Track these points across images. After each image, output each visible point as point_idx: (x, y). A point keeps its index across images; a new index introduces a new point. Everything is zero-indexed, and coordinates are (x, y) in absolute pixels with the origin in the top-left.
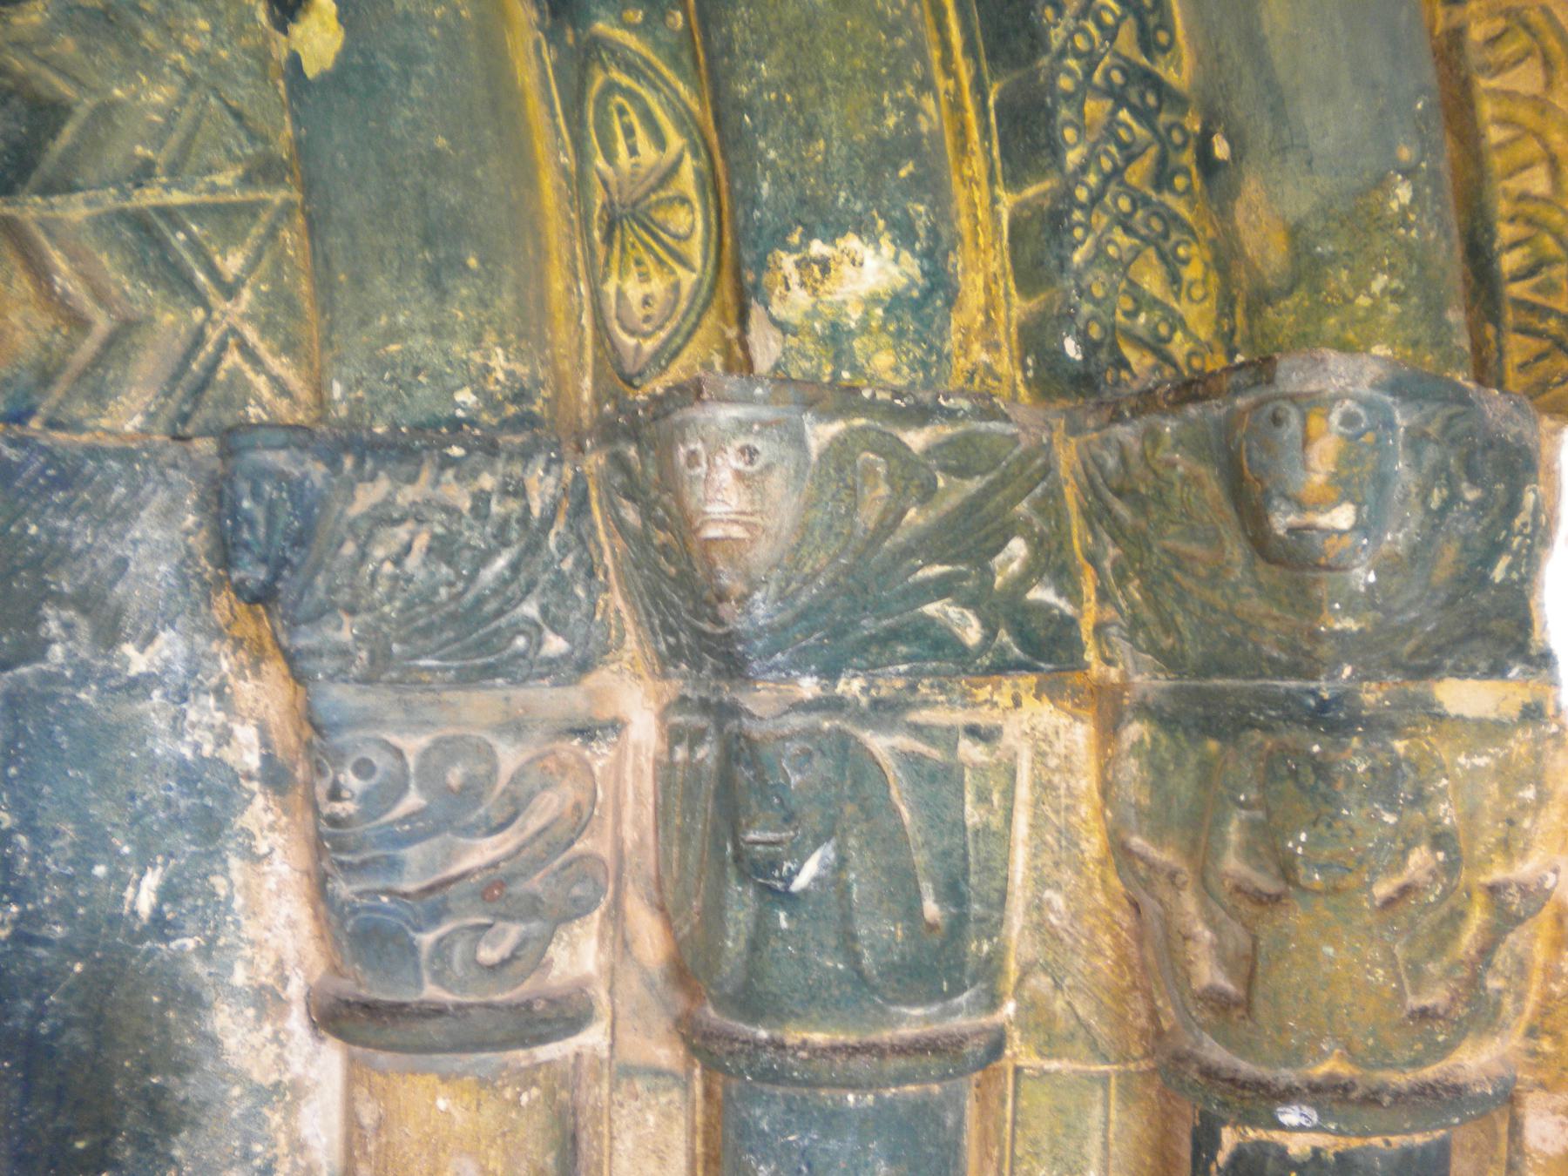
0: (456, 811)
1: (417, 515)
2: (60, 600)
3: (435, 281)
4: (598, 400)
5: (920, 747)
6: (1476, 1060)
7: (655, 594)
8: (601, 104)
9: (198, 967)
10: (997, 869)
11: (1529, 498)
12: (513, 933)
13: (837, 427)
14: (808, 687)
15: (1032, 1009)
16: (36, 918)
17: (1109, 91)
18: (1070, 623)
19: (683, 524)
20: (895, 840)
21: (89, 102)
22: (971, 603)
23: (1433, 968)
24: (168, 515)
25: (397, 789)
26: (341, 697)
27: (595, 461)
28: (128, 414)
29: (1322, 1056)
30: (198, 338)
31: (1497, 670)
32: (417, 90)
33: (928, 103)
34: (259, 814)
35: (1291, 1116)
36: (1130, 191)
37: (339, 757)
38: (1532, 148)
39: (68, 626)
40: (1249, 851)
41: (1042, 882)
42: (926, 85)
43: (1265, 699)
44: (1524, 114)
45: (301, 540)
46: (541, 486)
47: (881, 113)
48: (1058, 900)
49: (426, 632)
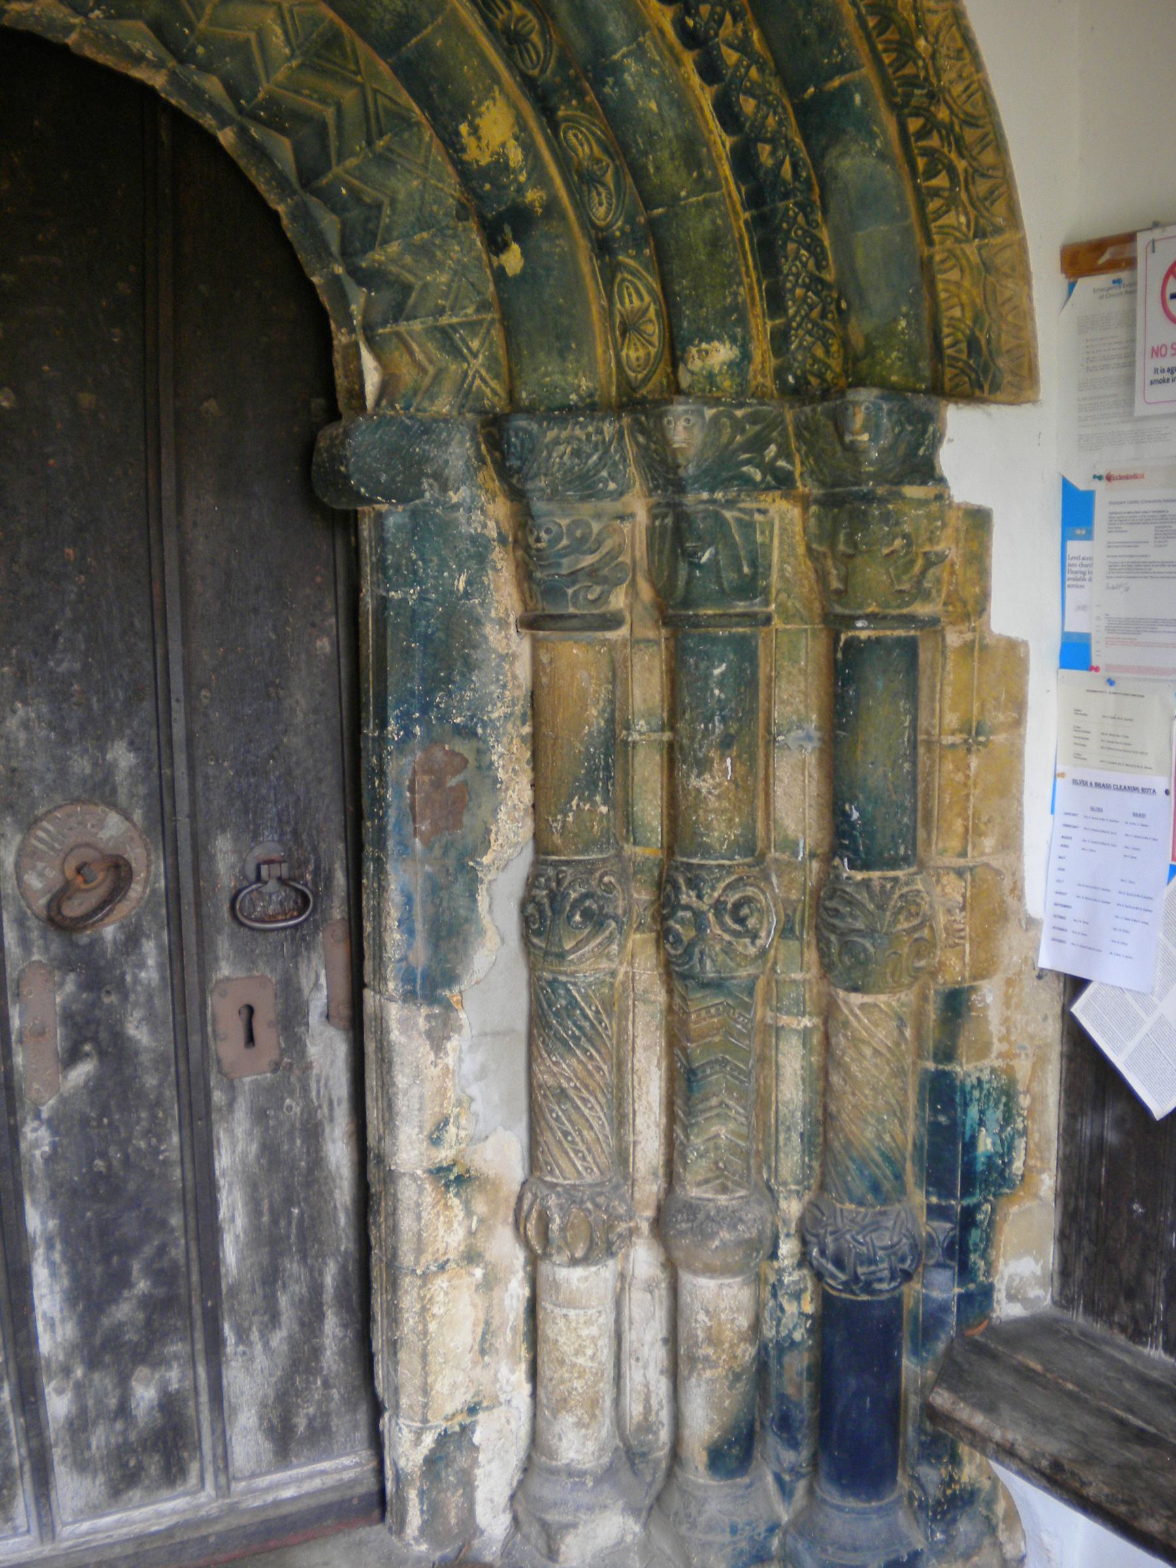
0: (580, 545)
1: (568, 442)
2: (428, 476)
3: (563, 359)
4: (619, 394)
5: (741, 515)
6: (922, 609)
7: (650, 467)
8: (620, 285)
9: (479, 610)
10: (768, 556)
11: (931, 429)
12: (598, 590)
13: (714, 411)
14: (705, 495)
15: (779, 606)
16: (426, 591)
17: (804, 286)
19: (665, 442)
20: (734, 545)
21: (420, 283)
22: (758, 466)
23: (905, 578)
24: (461, 443)
25: (559, 538)
27: (626, 420)
28: (443, 405)
29: (869, 605)
30: (466, 374)
31: (924, 483)
32: (552, 282)
33: (741, 290)
34: (498, 554)
35: (859, 624)
36: (811, 321)
38: (956, 300)
39: (431, 485)
40: (846, 543)
41: (782, 561)
42: (740, 283)
43: (850, 493)
44: (952, 288)
47: (725, 298)
48: (789, 569)
49: (570, 482)
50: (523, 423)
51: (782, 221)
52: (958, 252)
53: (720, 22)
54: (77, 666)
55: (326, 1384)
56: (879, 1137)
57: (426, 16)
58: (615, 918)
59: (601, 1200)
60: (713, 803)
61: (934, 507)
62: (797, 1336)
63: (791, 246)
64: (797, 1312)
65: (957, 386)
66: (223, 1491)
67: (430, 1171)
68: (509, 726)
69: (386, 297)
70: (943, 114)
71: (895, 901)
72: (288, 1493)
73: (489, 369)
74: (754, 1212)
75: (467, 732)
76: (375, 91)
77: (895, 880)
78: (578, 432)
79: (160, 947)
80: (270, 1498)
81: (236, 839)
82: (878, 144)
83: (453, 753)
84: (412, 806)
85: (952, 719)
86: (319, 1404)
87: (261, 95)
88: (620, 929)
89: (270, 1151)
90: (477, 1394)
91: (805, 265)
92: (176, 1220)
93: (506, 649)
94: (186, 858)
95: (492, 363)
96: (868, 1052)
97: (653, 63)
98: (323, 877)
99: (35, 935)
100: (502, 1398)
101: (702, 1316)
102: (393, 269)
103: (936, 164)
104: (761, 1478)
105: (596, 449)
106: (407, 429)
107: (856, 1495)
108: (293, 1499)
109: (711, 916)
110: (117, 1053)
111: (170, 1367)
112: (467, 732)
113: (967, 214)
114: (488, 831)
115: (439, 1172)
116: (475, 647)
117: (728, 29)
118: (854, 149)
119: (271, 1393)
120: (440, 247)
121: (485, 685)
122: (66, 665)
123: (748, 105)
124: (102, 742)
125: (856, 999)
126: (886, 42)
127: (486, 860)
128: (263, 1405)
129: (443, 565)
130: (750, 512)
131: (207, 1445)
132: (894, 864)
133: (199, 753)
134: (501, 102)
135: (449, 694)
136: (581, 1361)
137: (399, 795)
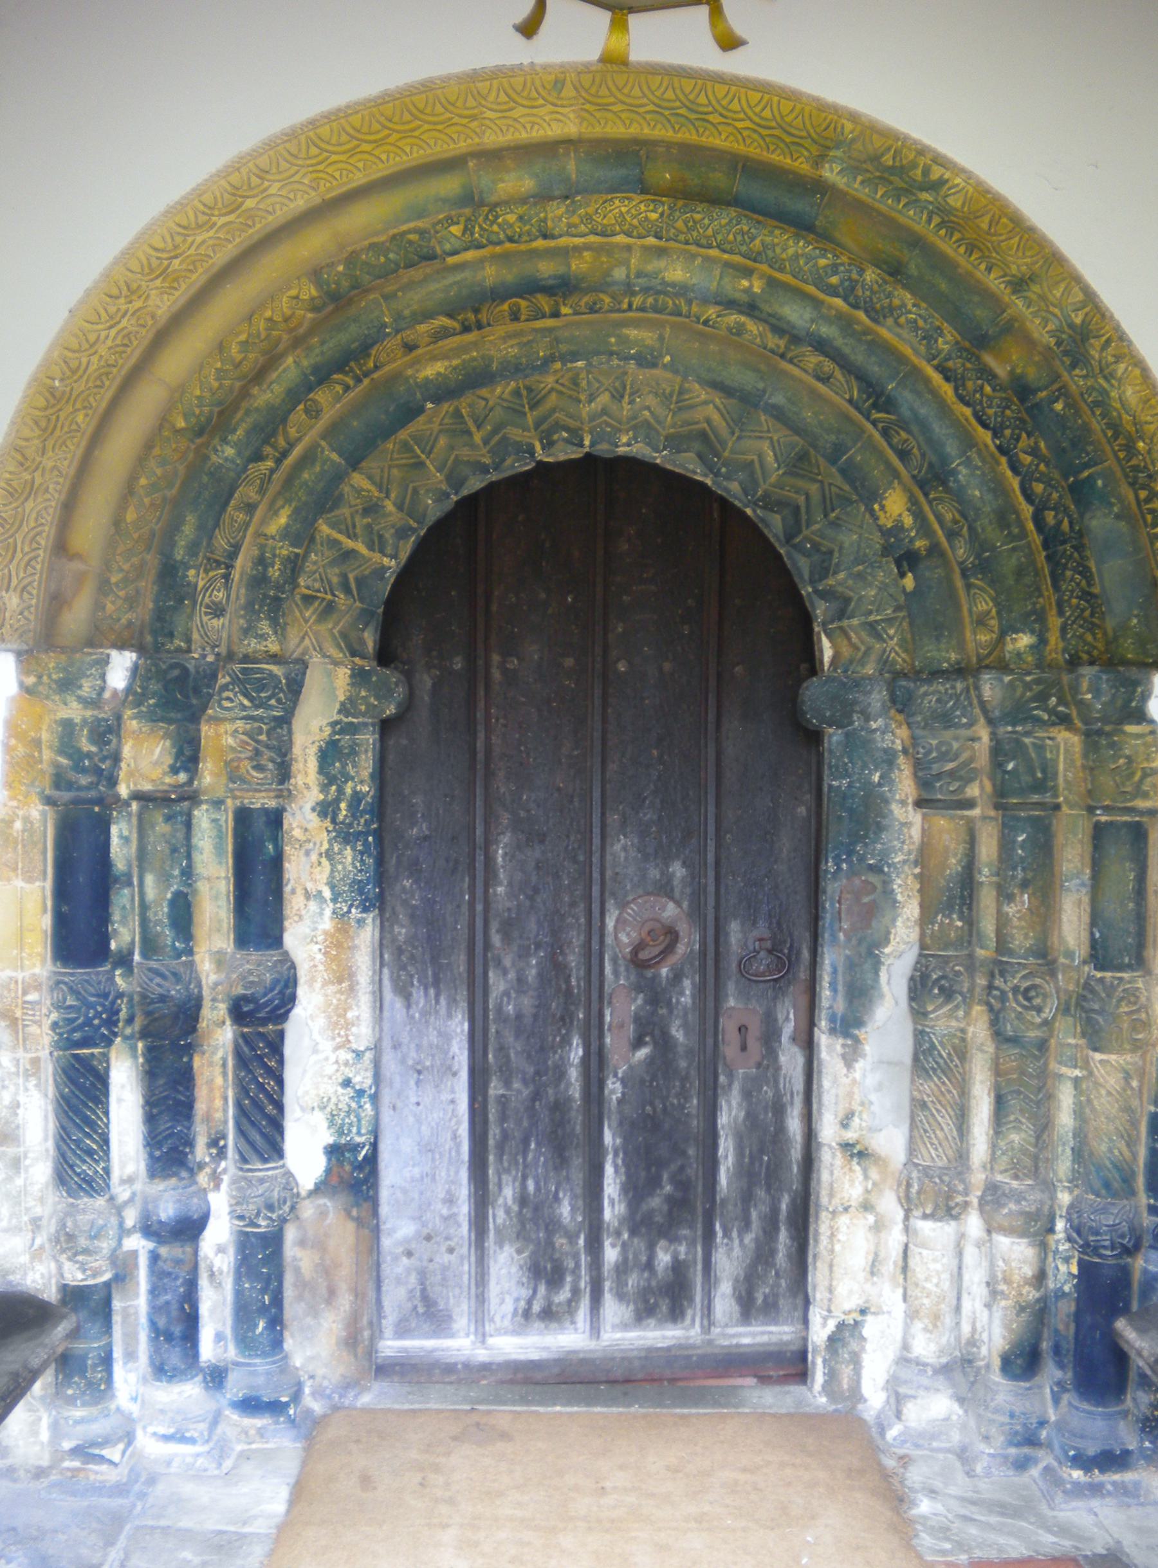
0: (944, 757)
1: (933, 693)
6: (1141, 804)
14: (1010, 728)
24: (880, 692)
25: (929, 752)
26: (919, 732)
28: (869, 670)
30: (884, 651)
31: (1139, 723)
34: (901, 760)
41: (1066, 770)
50: (904, 683)
53: (1018, 439)
54: (655, 817)
55: (777, 1274)
56: (1110, 1150)
58: (961, 994)
59: (946, 1178)
60: (1015, 922)
61: (1149, 739)
62: (1067, 1288)
63: (1069, 573)
64: (1065, 1272)
66: (706, 1329)
67: (840, 1145)
71: (1119, 993)
72: (746, 1341)
73: (901, 647)
74: (1036, 1196)
75: (876, 869)
77: (1121, 979)
78: (941, 688)
79: (693, 984)
80: (734, 1341)
81: (743, 924)
83: (866, 882)
84: (839, 913)
86: (772, 1287)
88: (964, 1001)
89: (751, 1117)
90: (867, 1301)
91: (1078, 584)
92: (691, 1152)
93: (907, 822)
94: (711, 932)
95: (903, 643)
96: (1103, 1092)
97: (977, 468)
98: (794, 952)
99: (622, 969)
100: (885, 1309)
101: (1001, 1263)
102: (840, 589)
104: (1040, 1387)
105: (951, 698)
106: (844, 684)
107: (1088, 1401)
108: (748, 1345)
109: (1010, 995)
110: (664, 1044)
111: (680, 1244)
112: (876, 869)
114: (889, 933)
115: (846, 1146)
117: (1024, 442)
119: (742, 1274)
122: (649, 815)
123: (1039, 488)
124: (667, 860)
125: (1098, 1056)
127: (887, 950)
128: (736, 1280)
129: (865, 766)
131: (698, 1298)
132: (1121, 968)
135: (866, 845)
136: (928, 1285)
137: (832, 905)
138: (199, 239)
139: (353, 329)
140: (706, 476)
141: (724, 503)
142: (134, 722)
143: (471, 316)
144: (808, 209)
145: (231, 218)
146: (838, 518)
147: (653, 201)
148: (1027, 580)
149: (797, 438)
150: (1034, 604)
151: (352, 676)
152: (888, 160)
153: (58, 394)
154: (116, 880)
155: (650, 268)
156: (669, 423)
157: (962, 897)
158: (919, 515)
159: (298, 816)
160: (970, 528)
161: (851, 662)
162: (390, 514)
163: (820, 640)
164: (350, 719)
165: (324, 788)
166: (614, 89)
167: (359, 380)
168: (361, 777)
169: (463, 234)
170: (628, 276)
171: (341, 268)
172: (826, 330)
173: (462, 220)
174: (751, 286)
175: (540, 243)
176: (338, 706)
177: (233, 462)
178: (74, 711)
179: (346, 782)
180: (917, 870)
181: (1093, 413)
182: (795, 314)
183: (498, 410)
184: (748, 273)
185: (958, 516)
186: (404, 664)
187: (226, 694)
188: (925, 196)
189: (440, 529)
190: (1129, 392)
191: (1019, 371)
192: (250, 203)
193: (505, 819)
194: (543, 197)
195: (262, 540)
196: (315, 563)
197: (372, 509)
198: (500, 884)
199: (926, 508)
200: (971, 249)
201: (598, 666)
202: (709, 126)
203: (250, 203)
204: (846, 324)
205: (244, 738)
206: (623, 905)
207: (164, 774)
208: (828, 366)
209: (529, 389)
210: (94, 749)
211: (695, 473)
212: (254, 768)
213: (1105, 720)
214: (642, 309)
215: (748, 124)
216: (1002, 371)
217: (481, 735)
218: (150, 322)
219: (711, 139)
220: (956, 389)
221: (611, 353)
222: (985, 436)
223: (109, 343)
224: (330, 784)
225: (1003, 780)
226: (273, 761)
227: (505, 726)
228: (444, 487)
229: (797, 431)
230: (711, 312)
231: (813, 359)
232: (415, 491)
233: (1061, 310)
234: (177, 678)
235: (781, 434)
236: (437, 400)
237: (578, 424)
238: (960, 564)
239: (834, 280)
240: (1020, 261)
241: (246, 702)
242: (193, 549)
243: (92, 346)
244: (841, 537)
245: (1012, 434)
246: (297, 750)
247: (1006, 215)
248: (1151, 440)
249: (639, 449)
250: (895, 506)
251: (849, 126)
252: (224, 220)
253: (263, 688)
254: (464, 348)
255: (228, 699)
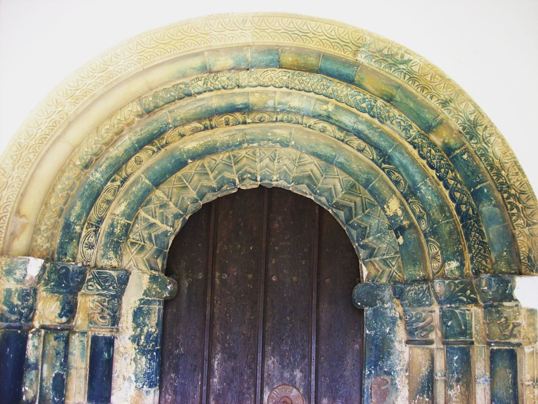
0: (418, 320)
2: (378, 300)
3: (414, 266)
6: (513, 341)
9: (393, 338)
11: (509, 285)
12: (425, 333)
14: (449, 306)
15: (476, 338)
17: (477, 244)
18: (476, 299)
22: (464, 297)
26: (406, 308)
28: (384, 280)
29: (495, 339)
30: (391, 272)
31: (510, 301)
34: (399, 322)
35: (492, 344)
37: (406, 314)
41: (475, 325)
44: (522, 242)
45: (402, 293)
46: (425, 287)
51: (469, 226)
52: (522, 231)
53: (448, 173)
57: (373, 179)
60: (454, 399)
61: (515, 309)
63: (473, 233)
65: (526, 271)
68: (402, 372)
69: (367, 252)
70: (513, 192)
73: (398, 270)
76: (365, 198)
82: (493, 202)
84: (371, 394)
85: (528, 376)
87: (334, 202)
91: (478, 238)
93: (402, 352)
95: (399, 268)
97: (430, 186)
102: (370, 244)
103: (513, 206)
106: (373, 287)
112: (388, 373)
113: (523, 220)
116: (391, 349)
117: (450, 175)
118: (486, 204)
120: (384, 237)
121: (394, 360)
123: (458, 195)
126: (494, 173)
129: (382, 324)
130: (464, 310)
133: (320, 375)
134: (395, 198)
135: (383, 362)
137: (368, 390)
138: (88, 82)
139: (155, 125)
140: (311, 195)
141: (321, 208)
142: (44, 293)
143: (208, 122)
144: (351, 73)
145: (103, 74)
146: (369, 213)
147: (285, 71)
148: (455, 237)
149: (351, 178)
150: (458, 248)
151: (150, 279)
152: (385, 52)
153: (22, 146)
154: (29, 366)
155: (284, 101)
156: (295, 173)
157: (428, 387)
158: (404, 210)
159: (123, 342)
160: (428, 215)
161: (376, 277)
162: (172, 208)
163: (362, 267)
164: (148, 298)
165: (135, 329)
166: (267, 23)
167: (159, 149)
168: (152, 325)
169: (203, 85)
170: (274, 104)
171: (151, 99)
172: (361, 127)
173: (203, 79)
174: (328, 108)
175: (237, 90)
176: (143, 292)
177: (99, 180)
178: (12, 285)
179: (145, 326)
180: (407, 374)
181: (481, 159)
182: (348, 120)
183: (221, 165)
184: (327, 103)
185: (422, 210)
186: (177, 275)
187: (90, 283)
188: (401, 66)
189: (195, 216)
190: (497, 149)
191: (446, 141)
192: (111, 68)
193: (219, 347)
194: (237, 69)
195: (113, 216)
196: (137, 228)
197: (163, 206)
198: (216, 377)
199: (408, 207)
200: (423, 88)
201: (263, 278)
202: (308, 38)
203: (111, 68)
204: (370, 125)
205: (98, 304)
206: (272, 390)
207: (56, 317)
208: (363, 144)
209: (234, 156)
210: (20, 303)
211: (306, 194)
212: (100, 317)
213: (494, 300)
214: (281, 121)
215: (325, 37)
216: (439, 142)
217: (208, 309)
218: (66, 117)
219: (309, 45)
220: (419, 151)
221: (269, 140)
222: (433, 173)
223: (47, 125)
224: (138, 327)
225: (446, 330)
226: (109, 314)
227: (220, 304)
228: (196, 196)
229: (350, 174)
230: (312, 121)
231: (357, 142)
232: (183, 198)
233: (464, 114)
234: (64, 273)
235: (344, 176)
236: (193, 159)
237: (255, 171)
238: (423, 231)
239: (364, 105)
240: (444, 93)
241: (99, 288)
242: (79, 217)
243: (39, 126)
244: (370, 221)
245: (445, 171)
246: (123, 311)
247: (438, 74)
248: (508, 171)
249: (282, 184)
250: (394, 206)
251: (368, 38)
252: (100, 75)
253: (107, 281)
254: (206, 137)
255: (91, 285)
